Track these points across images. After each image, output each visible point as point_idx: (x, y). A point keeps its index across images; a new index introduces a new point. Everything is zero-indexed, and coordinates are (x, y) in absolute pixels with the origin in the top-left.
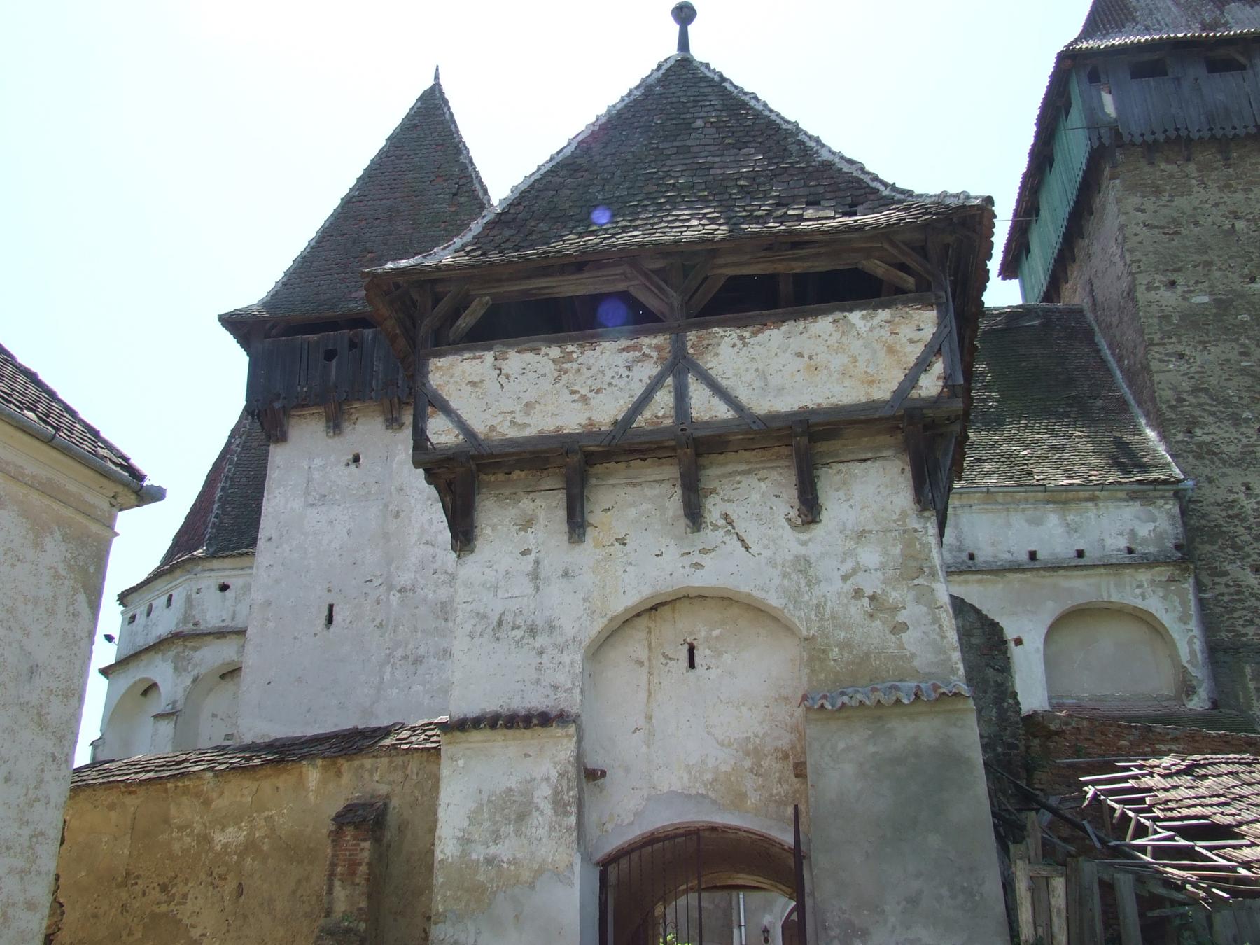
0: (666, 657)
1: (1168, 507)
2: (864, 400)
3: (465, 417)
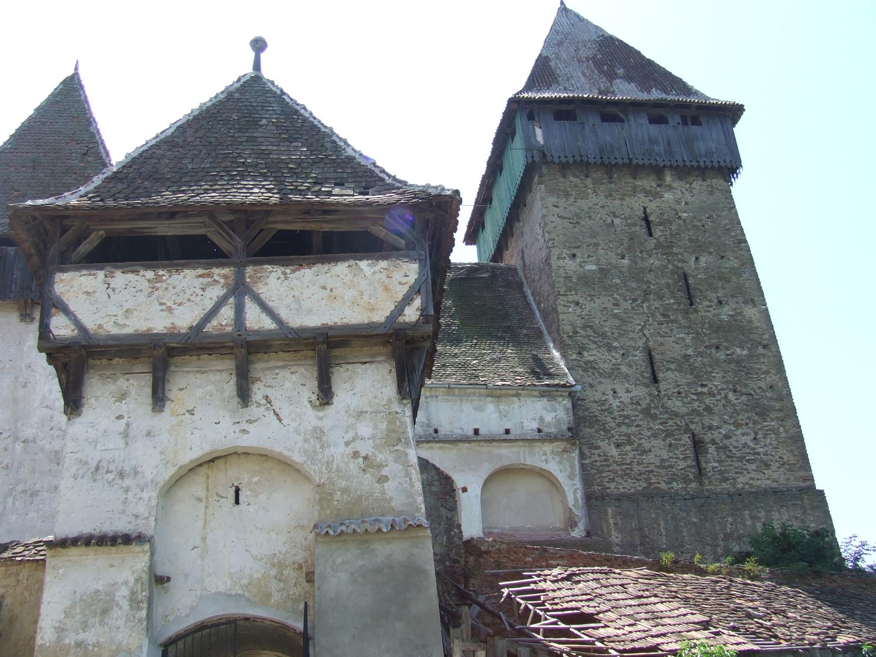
0: (218, 495)
1: (564, 402)
3: (80, 317)
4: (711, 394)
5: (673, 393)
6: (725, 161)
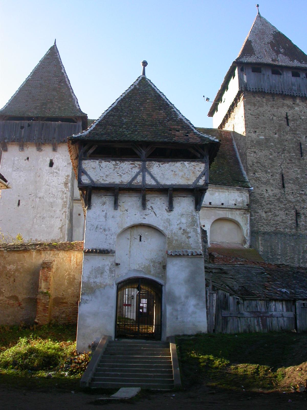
0: (134, 238)
1: (246, 194)
5: (290, 193)
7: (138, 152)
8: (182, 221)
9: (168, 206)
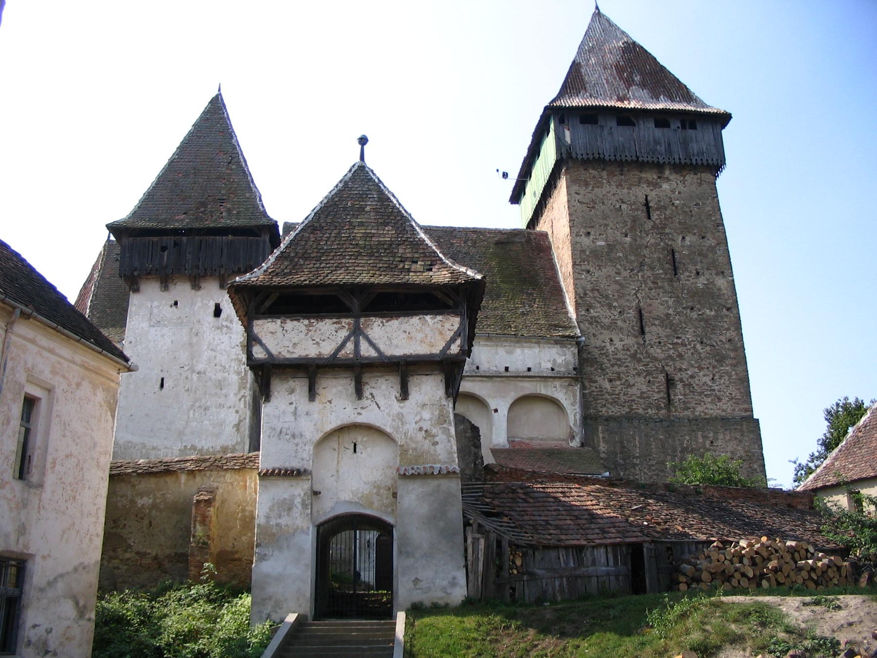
0: (345, 448)
1: (572, 349)
2: (429, 353)
3: (268, 347)
4: (683, 344)
6: (712, 160)
7: (348, 303)
8: (423, 417)
9: (400, 392)
